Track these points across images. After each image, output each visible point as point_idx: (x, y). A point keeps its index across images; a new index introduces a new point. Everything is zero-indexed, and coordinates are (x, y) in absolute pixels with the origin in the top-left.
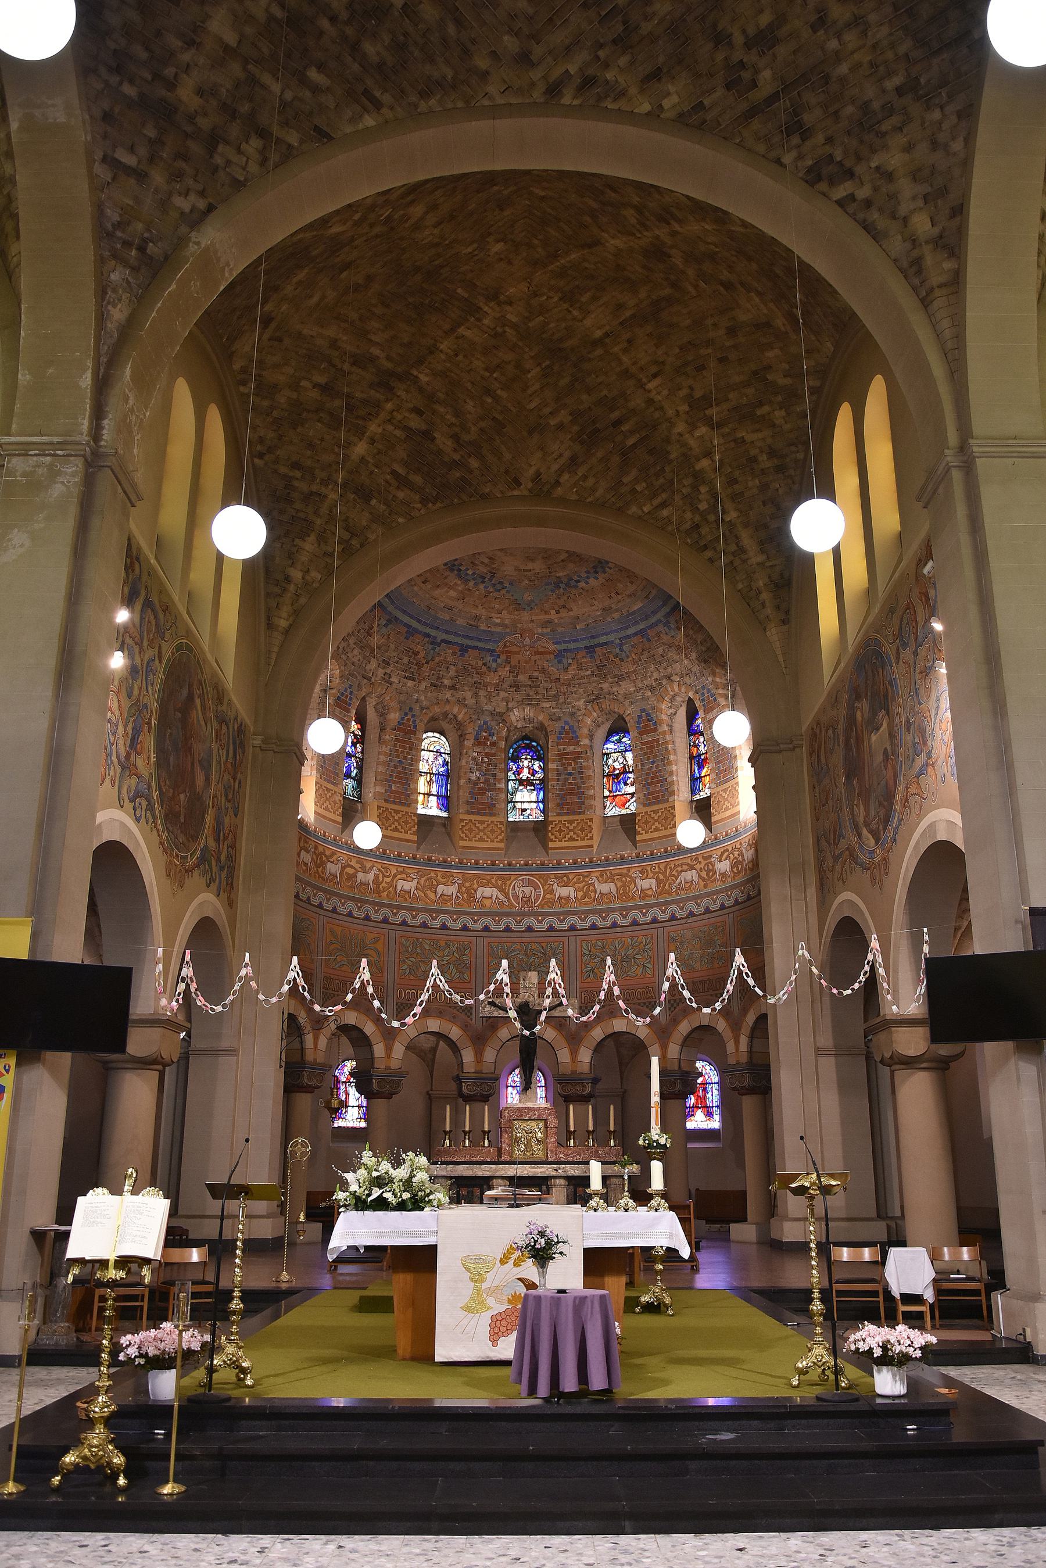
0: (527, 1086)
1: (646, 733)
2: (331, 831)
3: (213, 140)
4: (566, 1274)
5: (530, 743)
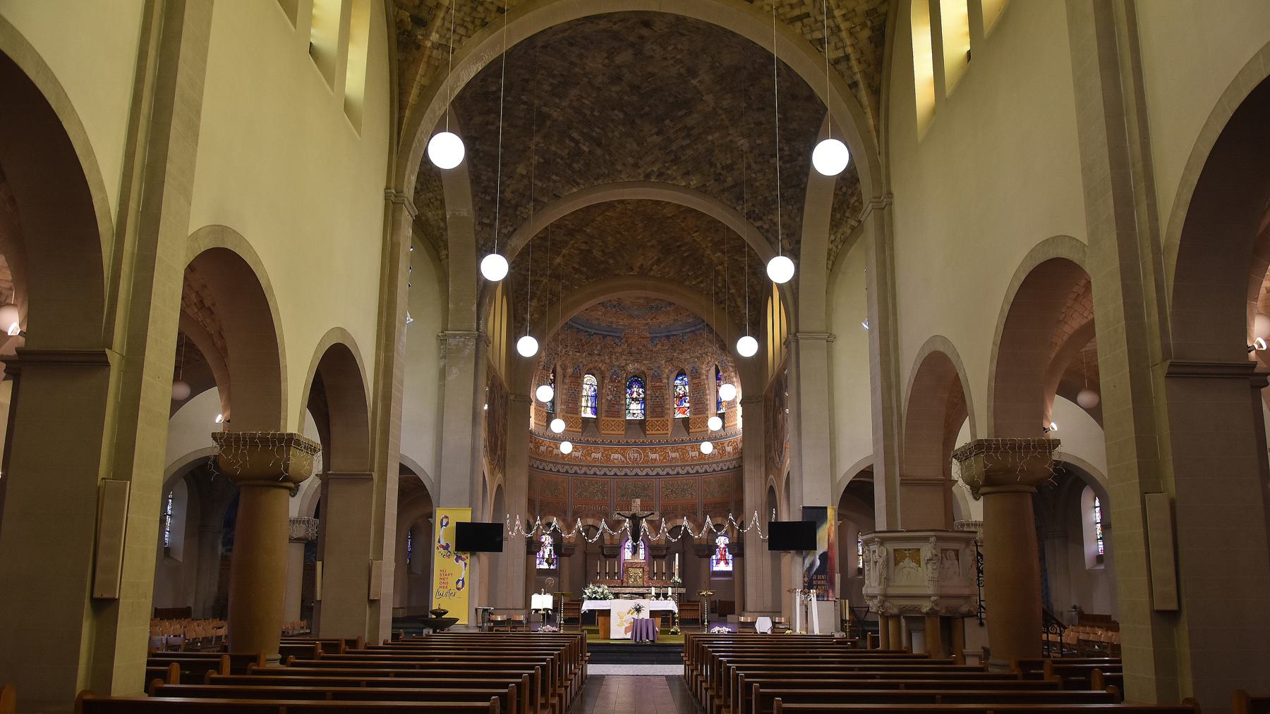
0: (635, 550)
1: (695, 376)
2: (541, 430)
3: (516, 206)
4: (645, 615)
5: (638, 379)
